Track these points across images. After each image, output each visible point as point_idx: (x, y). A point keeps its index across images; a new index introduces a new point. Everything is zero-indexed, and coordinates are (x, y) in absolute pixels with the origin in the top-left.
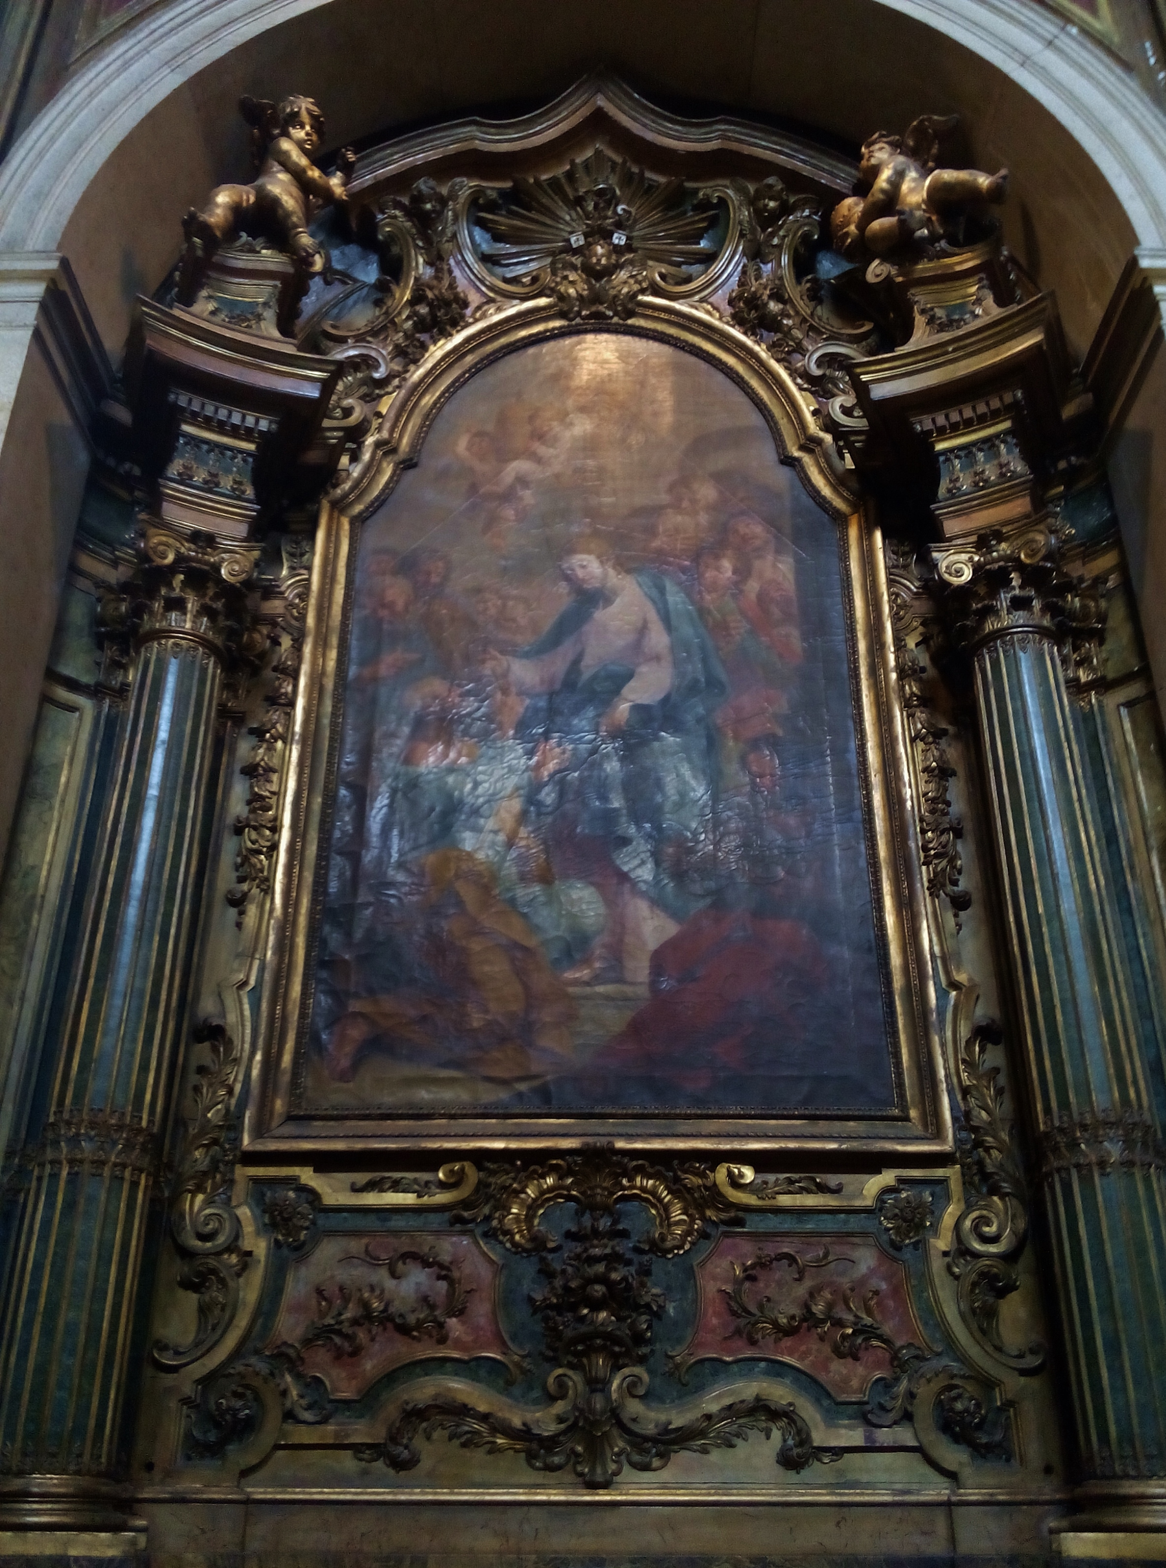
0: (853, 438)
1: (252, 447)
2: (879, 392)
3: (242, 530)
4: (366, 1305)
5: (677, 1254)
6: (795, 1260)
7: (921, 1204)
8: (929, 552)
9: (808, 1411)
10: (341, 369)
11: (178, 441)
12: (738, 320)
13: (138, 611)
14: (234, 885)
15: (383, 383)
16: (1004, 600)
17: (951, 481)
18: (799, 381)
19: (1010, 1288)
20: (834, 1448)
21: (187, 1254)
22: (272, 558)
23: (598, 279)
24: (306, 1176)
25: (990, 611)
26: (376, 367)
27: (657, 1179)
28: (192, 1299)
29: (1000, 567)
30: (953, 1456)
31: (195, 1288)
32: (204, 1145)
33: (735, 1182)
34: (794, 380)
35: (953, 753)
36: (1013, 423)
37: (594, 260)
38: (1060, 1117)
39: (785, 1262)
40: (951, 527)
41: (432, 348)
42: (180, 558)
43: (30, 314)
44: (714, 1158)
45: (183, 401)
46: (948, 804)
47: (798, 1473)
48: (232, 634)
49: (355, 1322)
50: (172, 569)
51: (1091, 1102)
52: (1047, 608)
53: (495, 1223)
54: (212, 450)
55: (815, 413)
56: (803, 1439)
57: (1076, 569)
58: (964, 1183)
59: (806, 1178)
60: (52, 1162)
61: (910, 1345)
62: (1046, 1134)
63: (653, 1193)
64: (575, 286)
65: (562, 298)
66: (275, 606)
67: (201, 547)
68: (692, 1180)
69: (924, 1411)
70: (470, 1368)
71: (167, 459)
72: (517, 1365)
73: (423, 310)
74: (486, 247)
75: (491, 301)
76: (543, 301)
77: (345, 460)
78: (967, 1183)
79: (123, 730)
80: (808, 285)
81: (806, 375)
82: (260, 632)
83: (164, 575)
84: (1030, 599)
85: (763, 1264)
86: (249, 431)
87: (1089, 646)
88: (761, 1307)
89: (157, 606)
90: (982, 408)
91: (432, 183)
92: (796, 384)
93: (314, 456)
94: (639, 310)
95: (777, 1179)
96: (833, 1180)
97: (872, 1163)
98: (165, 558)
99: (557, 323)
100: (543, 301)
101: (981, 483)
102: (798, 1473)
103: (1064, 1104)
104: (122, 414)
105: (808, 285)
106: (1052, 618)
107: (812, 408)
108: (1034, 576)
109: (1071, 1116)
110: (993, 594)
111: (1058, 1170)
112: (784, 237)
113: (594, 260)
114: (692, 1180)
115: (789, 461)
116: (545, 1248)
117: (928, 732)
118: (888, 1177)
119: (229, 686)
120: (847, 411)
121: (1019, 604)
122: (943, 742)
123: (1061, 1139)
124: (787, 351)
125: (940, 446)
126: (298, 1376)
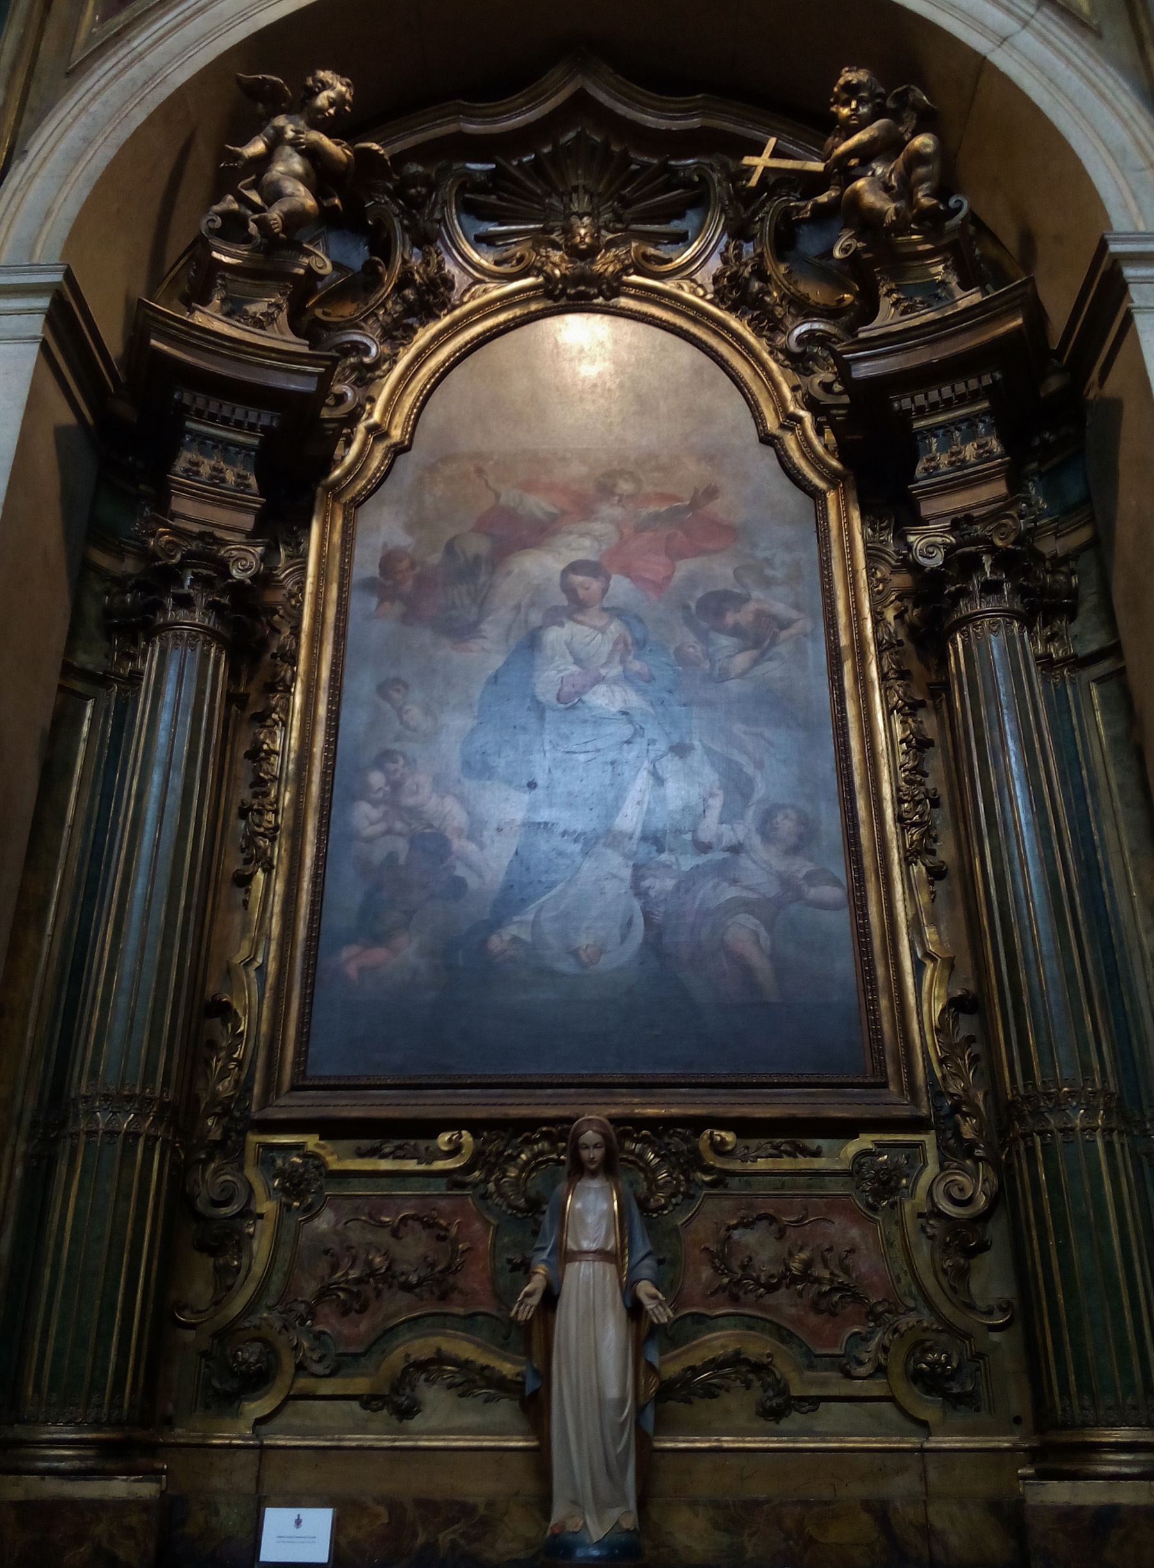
0: (834, 412)
2: (862, 371)
3: (247, 521)
5: (677, 1204)
7: (897, 1167)
9: (784, 1368)
11: (184, 437)
12: (720, 298)
15: (376, 365)
16: (975, 584)
17: (928, 461)
18: (781, 356)
19: (983, 1247)
20: (811, 1397)
21: (199, 1217)
24: (311, 1141)
25: (962, 593)
27: (644, 1143)
28: (208, 1263)
30: (929, 1411)
31: (213, 1252)
32: (215, 1114)
35: (930, 725)
37: (578, 239)
38: (1025, 1086)
39: (765, 1223)
40: (927, 508)
41: (421, 331)
44: (698, 1124)
46: (925, 775)
52: (1019, 590)
55: (794, 389)
56: (782, 1389)
58: (938, 1147)
59: (785, 1142)
62: (1013, 1103)
64: (557, 262)
65: (549, 278)
66: (279, 596)
71: (174, 456)
73: (409, 293)
75: (478, 281)
78: (941, 1147)
81: (786, 351)
84: (1000, 583)
86: (252, 427)
87: (1060, 624)
88: (744, 1267)
90: (960, 388)
96: (813, 1143)
97: (847, 1129)
103: (1028, 1073)
108: (1004, 560)
109: (1034, 1085)
110: (968, 578)
112: (767, 213)
115: (767, 439)
117: (906, 704)
118: (865, 1141)
119: (234, 674)
120: (827, 387)
121: (992, 588)
122: (921, 715)
123: (1027, 1108)
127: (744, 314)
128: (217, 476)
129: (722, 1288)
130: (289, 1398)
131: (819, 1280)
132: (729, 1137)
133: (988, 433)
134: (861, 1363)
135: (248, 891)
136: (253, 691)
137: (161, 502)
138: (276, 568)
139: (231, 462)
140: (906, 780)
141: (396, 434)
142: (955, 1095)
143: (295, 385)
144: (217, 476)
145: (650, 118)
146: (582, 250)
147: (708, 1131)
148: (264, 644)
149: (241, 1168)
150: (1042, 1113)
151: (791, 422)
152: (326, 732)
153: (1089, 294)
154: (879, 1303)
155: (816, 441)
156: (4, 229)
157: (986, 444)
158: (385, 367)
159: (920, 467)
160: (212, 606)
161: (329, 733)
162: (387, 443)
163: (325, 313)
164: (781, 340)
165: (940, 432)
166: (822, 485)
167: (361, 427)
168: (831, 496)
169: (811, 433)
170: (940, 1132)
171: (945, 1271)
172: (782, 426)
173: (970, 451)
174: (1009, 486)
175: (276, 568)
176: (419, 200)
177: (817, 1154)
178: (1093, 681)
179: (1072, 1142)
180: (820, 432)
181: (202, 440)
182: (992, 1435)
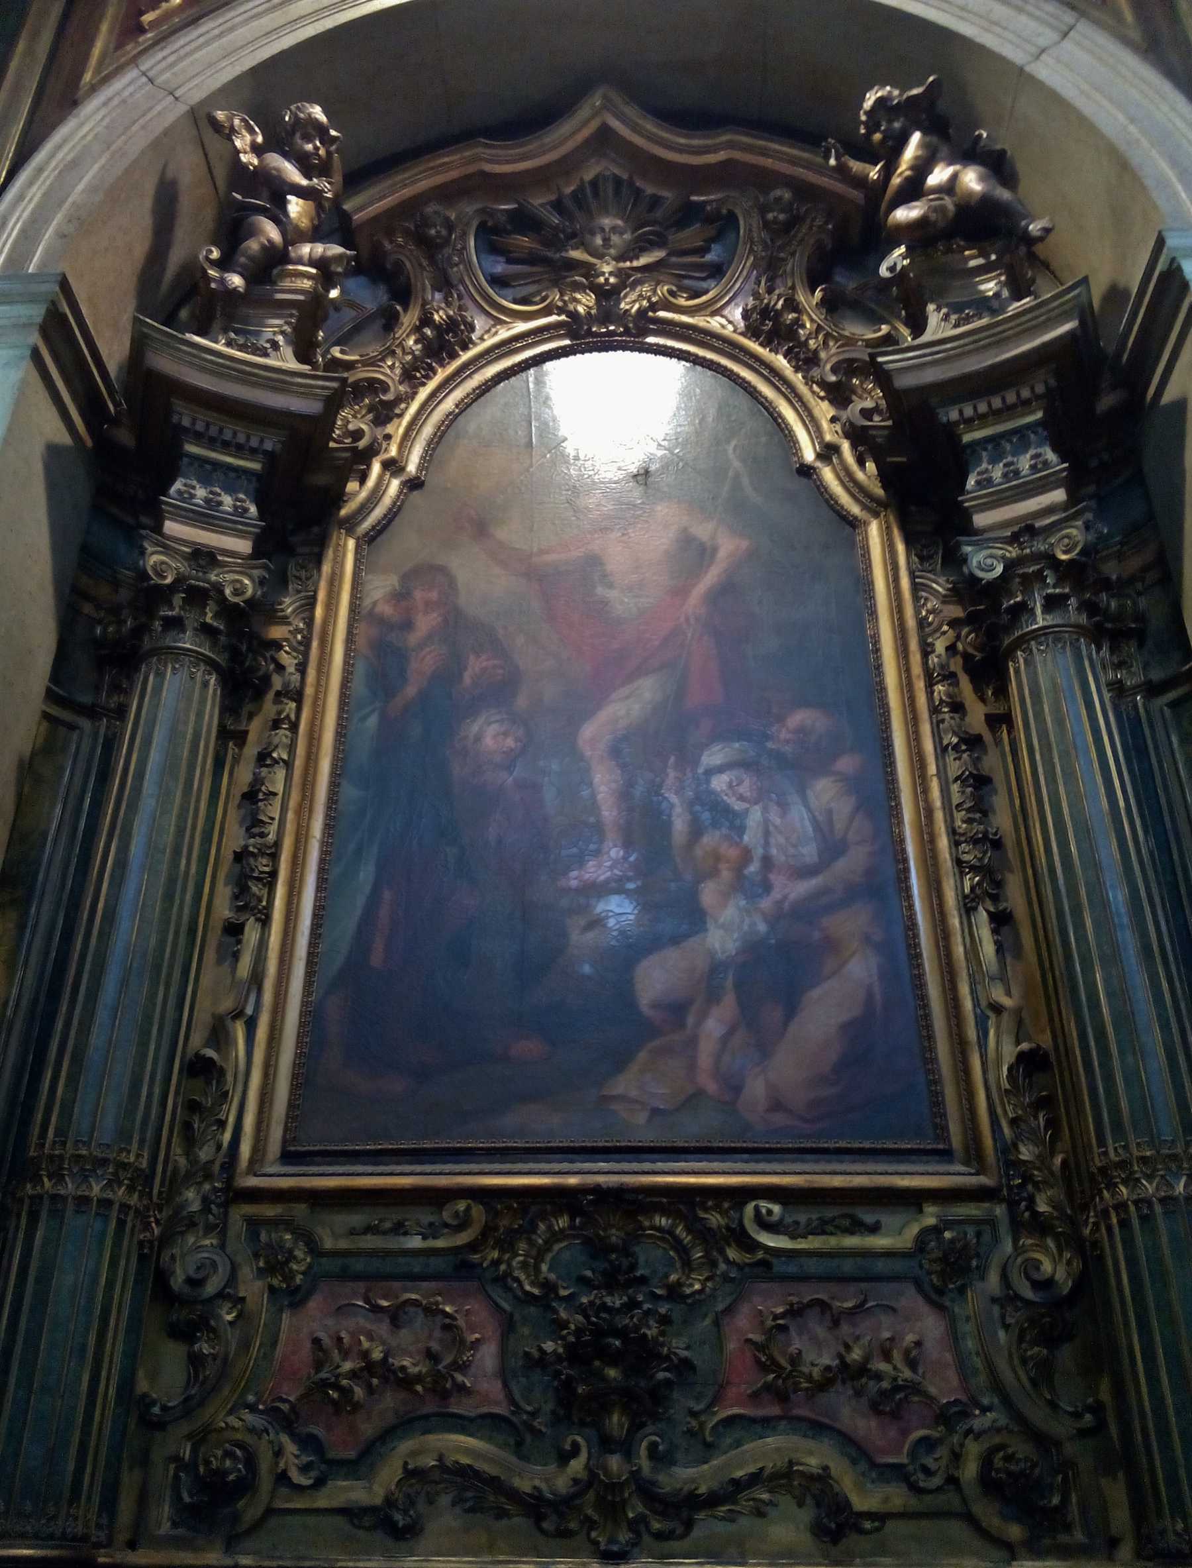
3: (244, 546)
6: (829, 1307)
8: (958, 545)
13: (140, 631)
18: (815, 387)
22: (278, 581)
32: (197, 1183)
36: (1045, 414)
42: (179, 580)
48: (235, 655)
49: (353, 1375)
50: (173, 588)
51: (1027, 1161)
53: (503, 1267)
54: (215, 470)
57: (1112, 570)
60: (32, 1198)
61: (798, 1303)
63: (671, 1232)
65: (573, 315)
67: (201, 567)
68: (715, 1220)
72: (524, 1422)
76: (553, 318)
77: (352, 486)
79: (120, 747)
83: (163, 594)
85: (795, 1312)
86: (254, 451)
89: (157, 625)
91: (440, 208)
92: (813, 392)
93: (321, 479)
95: (810, 1220)
98: (165, 578)
100: (553, 318)
104: (125, 437)
106: (1090, 617)
107: (829, 417)
113: (602, 280)
114: (715, 1220)
118: (930, 1216)
124: (806, 361)
125: (967, 438)
126: (293, 1435)
128: (212, 503)
129: (768, 1387)
130: (270, 1512)
131: (878, 1376)
132: (776, 1209)
133: (1040, 445)
135: (239, 942)
139: (230, 490)
141: (412, 468)
142: (1030, 1162)
143: (297, 405)
144: (212, 503)
147: (753, 1204)
148: (266, 680)
150: (1138, 1180)
151: (828, 452)
155: (860, 476)
159: (971, 482)
160: (207, 630)
163: (342, 352)
164: (815, 373)
166: (856, 510)
167: (376, 468)
168: (874, 530)
170: (1012, 1206)
171: (1024, 1361)
172: (819, 456)
174: (1070, 493)
176: (438, 241)
177: (874, 1229)
180: (861, 462)
181: (208, 472)
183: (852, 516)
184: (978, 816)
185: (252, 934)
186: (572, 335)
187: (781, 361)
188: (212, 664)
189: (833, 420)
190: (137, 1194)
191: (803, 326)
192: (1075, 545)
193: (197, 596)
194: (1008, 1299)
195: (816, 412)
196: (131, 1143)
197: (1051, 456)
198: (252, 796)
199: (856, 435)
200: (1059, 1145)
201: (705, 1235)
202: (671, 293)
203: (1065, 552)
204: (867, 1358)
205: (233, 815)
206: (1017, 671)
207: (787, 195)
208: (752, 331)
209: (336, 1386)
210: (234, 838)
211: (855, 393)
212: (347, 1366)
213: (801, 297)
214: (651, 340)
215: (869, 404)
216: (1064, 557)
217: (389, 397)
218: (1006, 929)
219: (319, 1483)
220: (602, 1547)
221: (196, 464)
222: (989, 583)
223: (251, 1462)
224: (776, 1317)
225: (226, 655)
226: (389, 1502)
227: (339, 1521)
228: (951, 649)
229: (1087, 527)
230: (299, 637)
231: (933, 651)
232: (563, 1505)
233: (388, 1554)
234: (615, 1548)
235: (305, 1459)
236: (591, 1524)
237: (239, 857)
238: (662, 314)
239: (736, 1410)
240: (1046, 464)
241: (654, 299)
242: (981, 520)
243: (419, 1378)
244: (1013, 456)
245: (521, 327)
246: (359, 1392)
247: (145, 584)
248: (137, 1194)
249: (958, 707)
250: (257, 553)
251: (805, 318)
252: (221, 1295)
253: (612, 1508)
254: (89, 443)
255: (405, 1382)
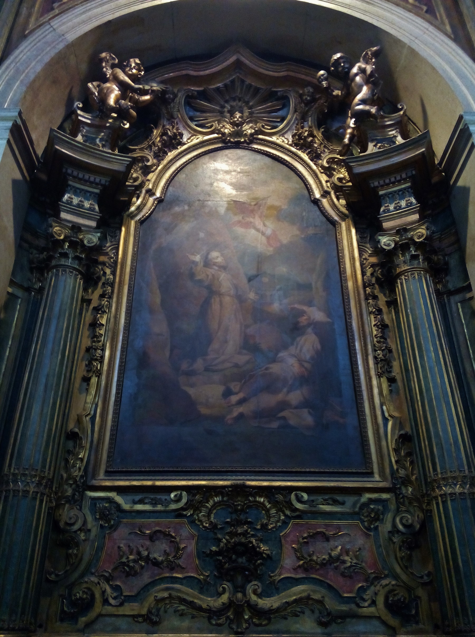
1: (97, 191)
4: (139, 553)
10: (135, 161)
13: (50, 258)
14: (85, 373)
23: (237, 127)
26: (148, 161)
29: (406, 243)
33: (299, 500)
34: (318, 168)
43: (7, 135)
45: (69, 171)
47: (153, 627)
50: (64, 241)
64: (228, 129)
65: (224, 134)
68: (280, 497)
69: (380, 600)
70: (188, 581)
74: (191, 114)
76: (216, 135)
77: (134, 199)
80: (323, 130)
81: (323, 167)
82: (98, 268)
94: (255, 141)
99: (220, 145)
100: (216, 135)
101: (398, 208)
102: (153, 627)
104: (43, 177)
105: (323, 130)
111: (441, 495)
114: (280, 497)
116: (217, 528)
124: (315, 157)
125: (381, 193)
127: (305, 150)
129: (299, 566)
134: (364, 600)
136: (95, 297)
137: (57, 215)
138: (105, 246)
140: (377, 342)
142: (403, 477)
145: (157, 578)
146: (237, 123)
149: (80, 509)
151: (325, 194)
152: (126, 315)
153: (449, 148)
154: (372, 573)
156: (1, 82)
157: (409, 200)
158: (154, 168)
159: (382, 209)
160: (76, 258)
161: (127, 316)
162: (155, 197)
165: (390, 196)
166: (336, 218)
168: (343, 224)
169: (335, 200)
173: (403, 203)
175: (105, 246)
178: (459, 302)
179: (455, 499)
180: (338, 199)
182: (461, 397)
183: (335, 220)
184: (382, 340)
185: (94, 380)
186: (224, 141)
187: (305, 157)
188: (80, 272)
189: (327, 182)
190: (48, 488)
191: (315, 143)
192: (422, 236)
193: (73, 245)
194: (395, 531)
195: (322, 179)
196: (45, 469)
197: (414, 201)
198: (94, 325)
199: (336, 189)
200: (415, 472)
201: (275, 504)
202: (263, 126)
203: (418, 239)
204: (340, 555)
205: (87, 333)
206: (402, 284)
207: (311, 90)
208: (295, 144)
209: (128, 566)
210: (86, 342)
211: (335, 171)
212: (131, 557)
213: (315, 133)
214: (255, 146)
215: (342, 176)
216: (418, 240)
217: (149, 164)
218: (393, 385)
219: (121, 604)
220: (235, 630)
221: (73, 189)
222: (389, 250)
223: (93, 596)
224: (304, 538)
225: (85, 268)
226: (149, 612)
227: (130, 620)
228: (372, 274)
229: (427, 229)
230: (112, 260)
231: (366, 275)
232: (220, 612)
233: (148, 633)
234: (239, 630)
235: (115, 594)
236: (232, 621)
237: (88, 350)
238: (260, 137)
239: (289, 575)
240: (411, 203)
241: (256, 129)
242: (386, 225)
243: (162, 562)
244: (399, 200)
245: (201, 138)
246: (137, 567)
247: (52, 239)
248: (48, 488)
249: (375, 298)
250: (98, 227)
251: (316, 139)
252: (80, 529)
253: (239, 614)
254: (28, 178)
255: (156, 564)
